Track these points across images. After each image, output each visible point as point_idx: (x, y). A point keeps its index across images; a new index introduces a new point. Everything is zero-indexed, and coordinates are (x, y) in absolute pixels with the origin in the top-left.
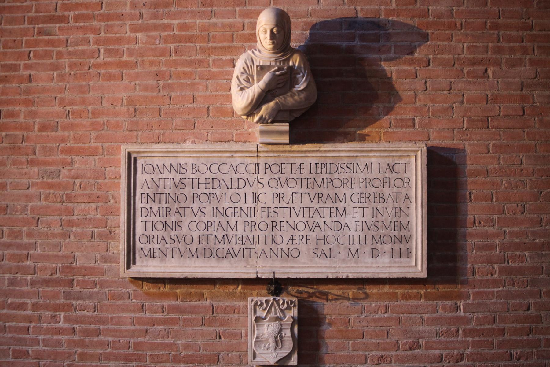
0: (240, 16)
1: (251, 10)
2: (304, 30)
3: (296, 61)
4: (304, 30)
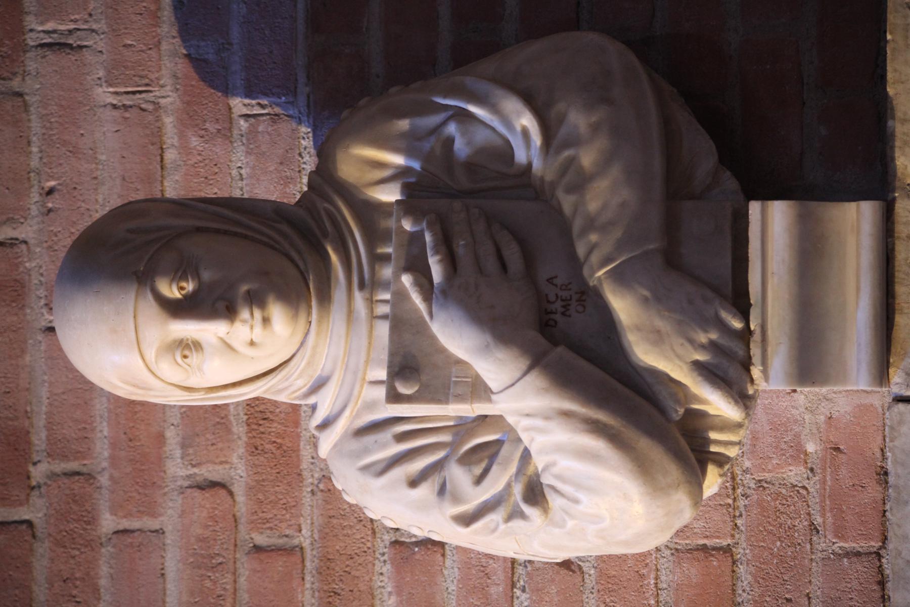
0: (151, 510)
1: (114, 445)
2: (226, 133)
3: (377, 166)
4: (226, 133)
